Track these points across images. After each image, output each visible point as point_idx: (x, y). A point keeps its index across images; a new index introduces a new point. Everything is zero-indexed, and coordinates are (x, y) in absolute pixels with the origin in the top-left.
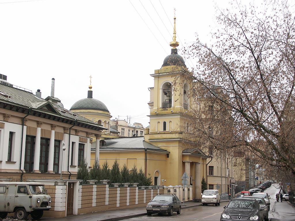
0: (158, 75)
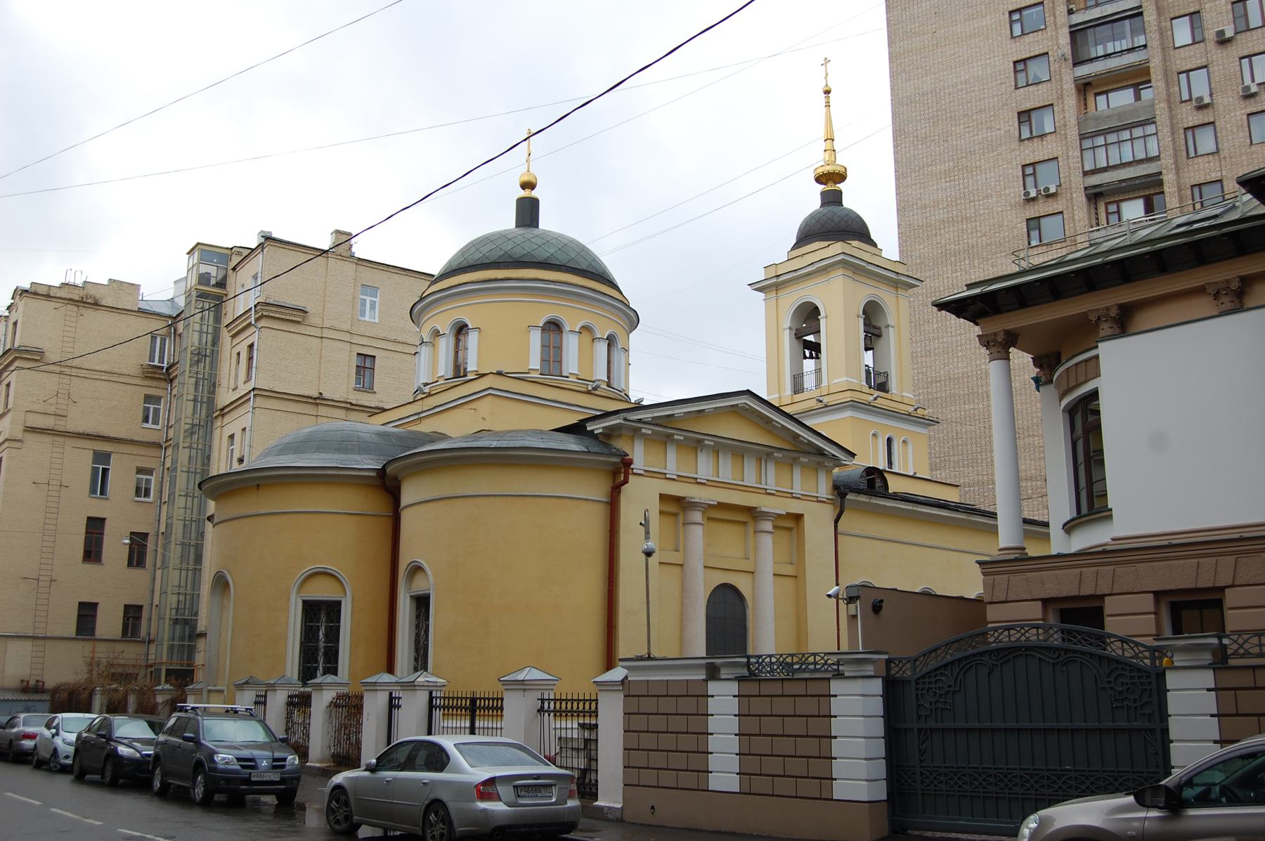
0: (774, 280)
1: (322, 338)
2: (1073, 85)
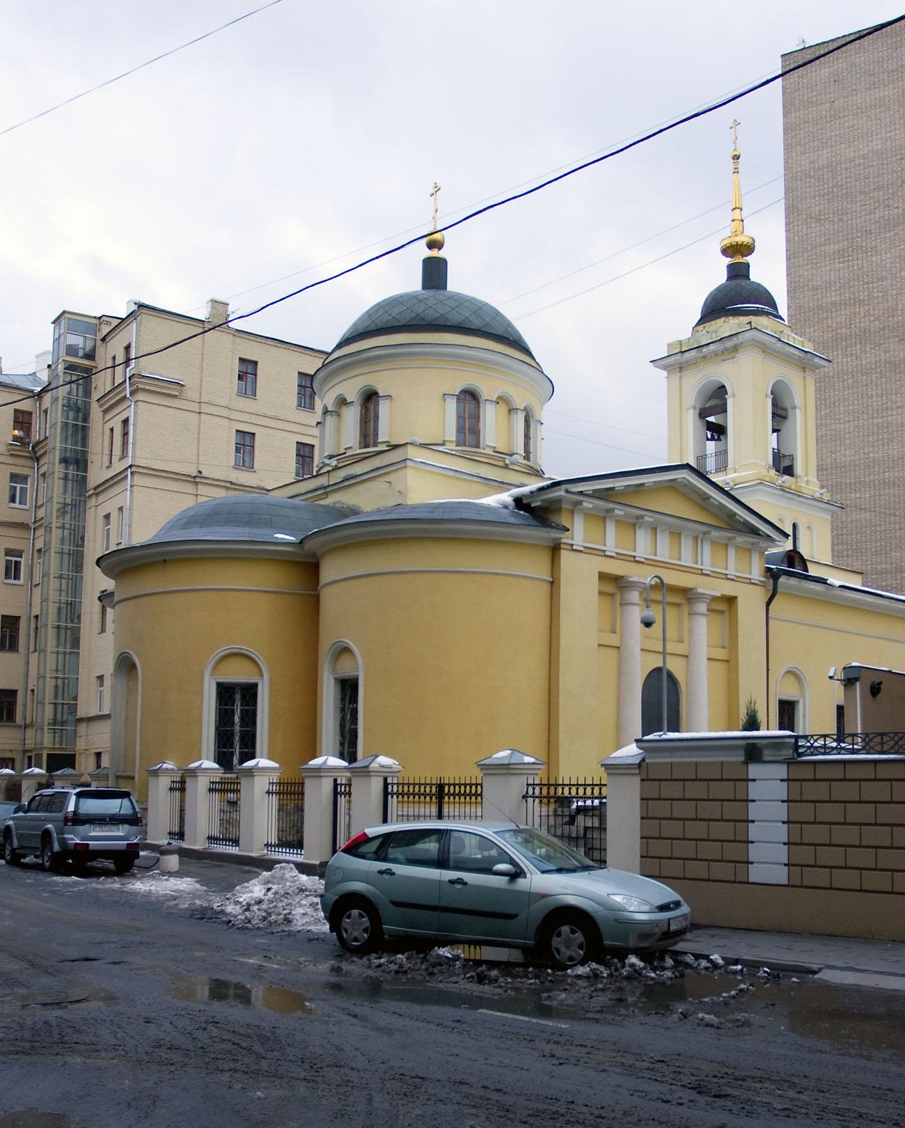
1: (200, 413)
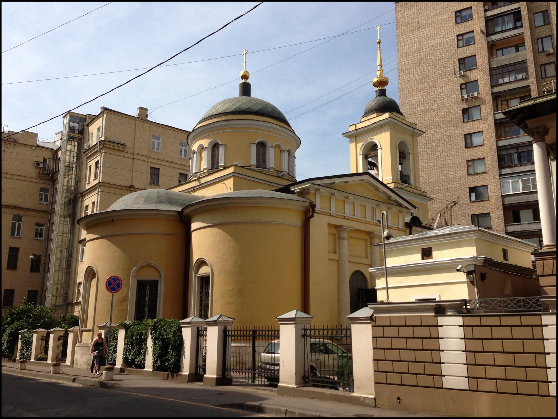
2: (486, 45)
